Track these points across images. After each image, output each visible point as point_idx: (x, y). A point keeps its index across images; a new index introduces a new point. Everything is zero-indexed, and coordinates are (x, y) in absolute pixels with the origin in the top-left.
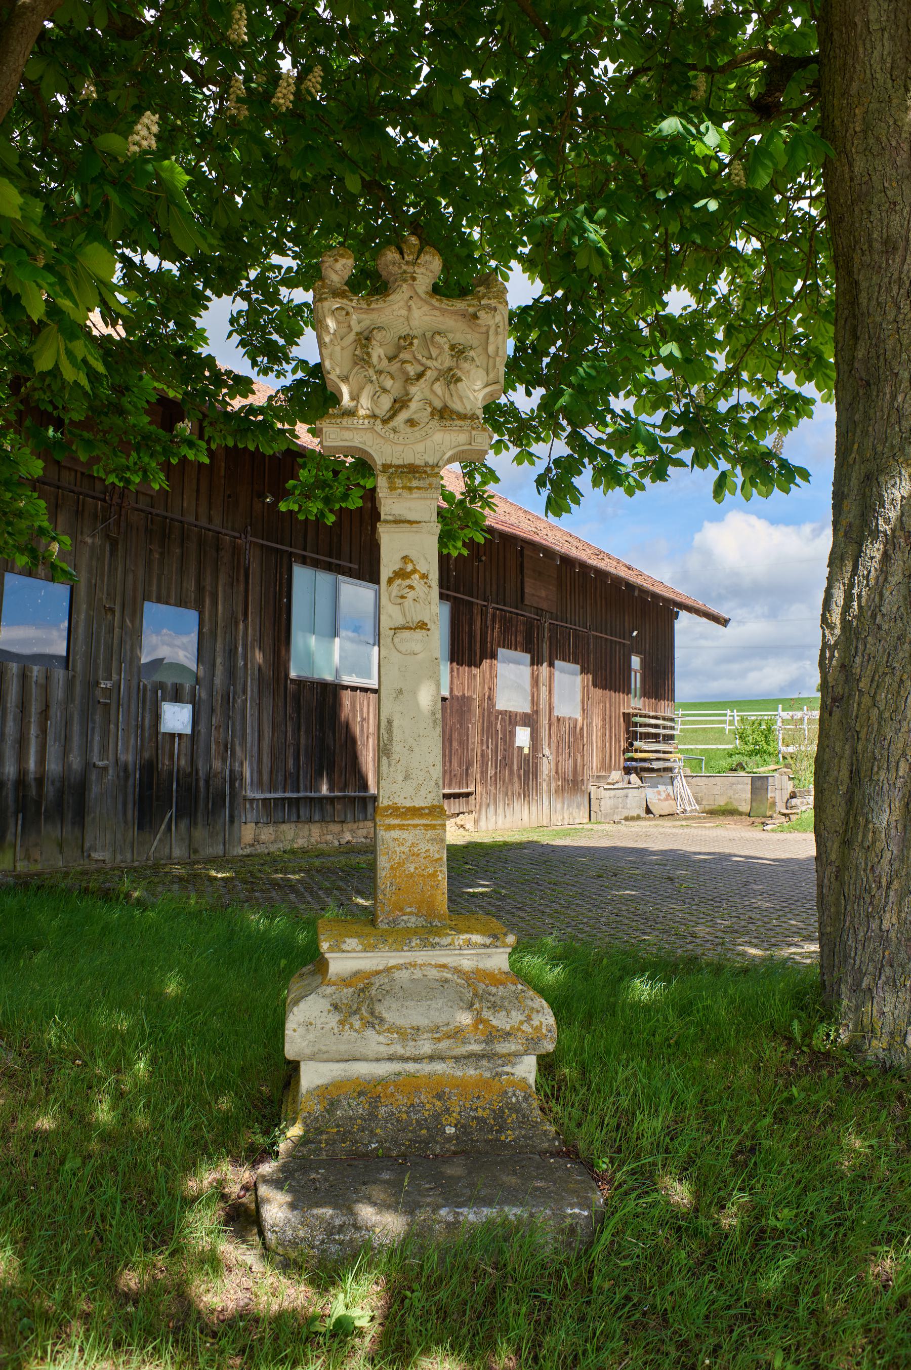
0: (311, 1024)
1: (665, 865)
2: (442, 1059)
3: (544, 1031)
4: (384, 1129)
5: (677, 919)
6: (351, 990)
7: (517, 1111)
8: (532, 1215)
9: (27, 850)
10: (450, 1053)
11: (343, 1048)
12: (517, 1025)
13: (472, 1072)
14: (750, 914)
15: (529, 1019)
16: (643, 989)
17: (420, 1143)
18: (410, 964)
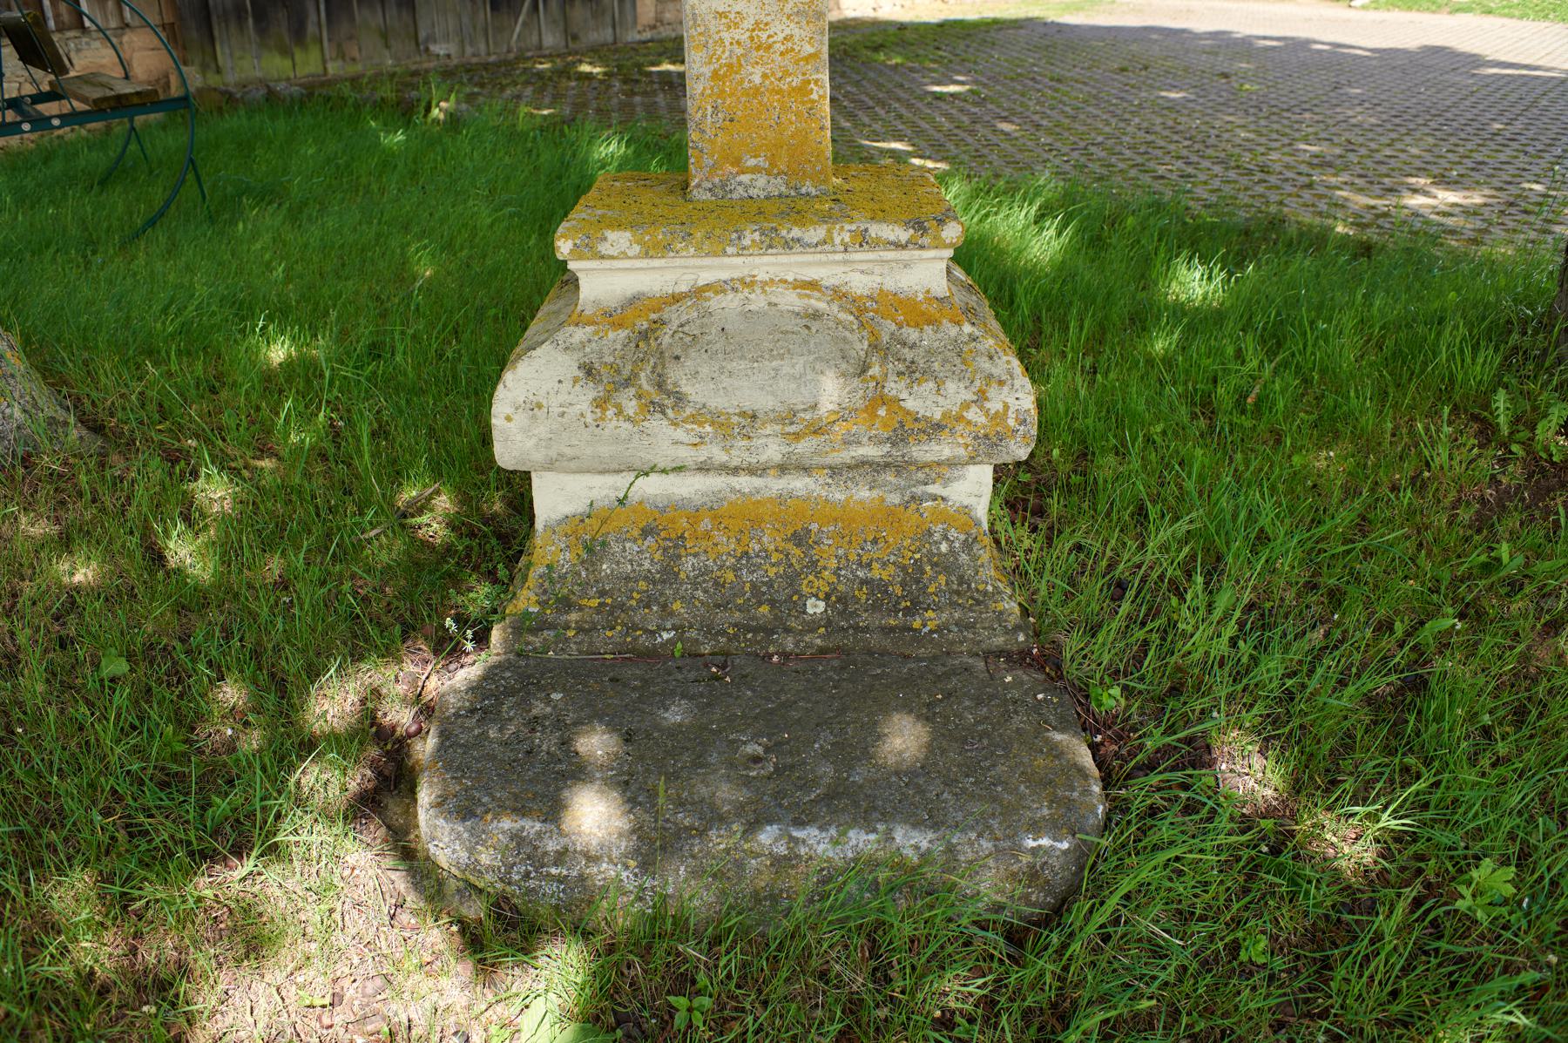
0: (540, 406)
1: (1216, 54)
2: (806, 470)
3: (1011, 422)
4: (689, 601)
5: (1239, 141)
6: (623, 334)
7: (947, 570)
8: (951, 850)
9: (339, 46)
10: (817, 460)
11: (605, 450)
12: (955, 409)
13: (864, 493)
14: (1347, 135)
15: (982, 397)
16: (1193, 283)
17: (755, 630)
18: (742, 281)
